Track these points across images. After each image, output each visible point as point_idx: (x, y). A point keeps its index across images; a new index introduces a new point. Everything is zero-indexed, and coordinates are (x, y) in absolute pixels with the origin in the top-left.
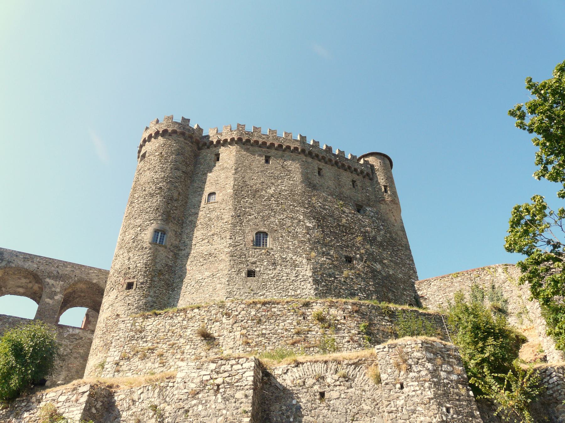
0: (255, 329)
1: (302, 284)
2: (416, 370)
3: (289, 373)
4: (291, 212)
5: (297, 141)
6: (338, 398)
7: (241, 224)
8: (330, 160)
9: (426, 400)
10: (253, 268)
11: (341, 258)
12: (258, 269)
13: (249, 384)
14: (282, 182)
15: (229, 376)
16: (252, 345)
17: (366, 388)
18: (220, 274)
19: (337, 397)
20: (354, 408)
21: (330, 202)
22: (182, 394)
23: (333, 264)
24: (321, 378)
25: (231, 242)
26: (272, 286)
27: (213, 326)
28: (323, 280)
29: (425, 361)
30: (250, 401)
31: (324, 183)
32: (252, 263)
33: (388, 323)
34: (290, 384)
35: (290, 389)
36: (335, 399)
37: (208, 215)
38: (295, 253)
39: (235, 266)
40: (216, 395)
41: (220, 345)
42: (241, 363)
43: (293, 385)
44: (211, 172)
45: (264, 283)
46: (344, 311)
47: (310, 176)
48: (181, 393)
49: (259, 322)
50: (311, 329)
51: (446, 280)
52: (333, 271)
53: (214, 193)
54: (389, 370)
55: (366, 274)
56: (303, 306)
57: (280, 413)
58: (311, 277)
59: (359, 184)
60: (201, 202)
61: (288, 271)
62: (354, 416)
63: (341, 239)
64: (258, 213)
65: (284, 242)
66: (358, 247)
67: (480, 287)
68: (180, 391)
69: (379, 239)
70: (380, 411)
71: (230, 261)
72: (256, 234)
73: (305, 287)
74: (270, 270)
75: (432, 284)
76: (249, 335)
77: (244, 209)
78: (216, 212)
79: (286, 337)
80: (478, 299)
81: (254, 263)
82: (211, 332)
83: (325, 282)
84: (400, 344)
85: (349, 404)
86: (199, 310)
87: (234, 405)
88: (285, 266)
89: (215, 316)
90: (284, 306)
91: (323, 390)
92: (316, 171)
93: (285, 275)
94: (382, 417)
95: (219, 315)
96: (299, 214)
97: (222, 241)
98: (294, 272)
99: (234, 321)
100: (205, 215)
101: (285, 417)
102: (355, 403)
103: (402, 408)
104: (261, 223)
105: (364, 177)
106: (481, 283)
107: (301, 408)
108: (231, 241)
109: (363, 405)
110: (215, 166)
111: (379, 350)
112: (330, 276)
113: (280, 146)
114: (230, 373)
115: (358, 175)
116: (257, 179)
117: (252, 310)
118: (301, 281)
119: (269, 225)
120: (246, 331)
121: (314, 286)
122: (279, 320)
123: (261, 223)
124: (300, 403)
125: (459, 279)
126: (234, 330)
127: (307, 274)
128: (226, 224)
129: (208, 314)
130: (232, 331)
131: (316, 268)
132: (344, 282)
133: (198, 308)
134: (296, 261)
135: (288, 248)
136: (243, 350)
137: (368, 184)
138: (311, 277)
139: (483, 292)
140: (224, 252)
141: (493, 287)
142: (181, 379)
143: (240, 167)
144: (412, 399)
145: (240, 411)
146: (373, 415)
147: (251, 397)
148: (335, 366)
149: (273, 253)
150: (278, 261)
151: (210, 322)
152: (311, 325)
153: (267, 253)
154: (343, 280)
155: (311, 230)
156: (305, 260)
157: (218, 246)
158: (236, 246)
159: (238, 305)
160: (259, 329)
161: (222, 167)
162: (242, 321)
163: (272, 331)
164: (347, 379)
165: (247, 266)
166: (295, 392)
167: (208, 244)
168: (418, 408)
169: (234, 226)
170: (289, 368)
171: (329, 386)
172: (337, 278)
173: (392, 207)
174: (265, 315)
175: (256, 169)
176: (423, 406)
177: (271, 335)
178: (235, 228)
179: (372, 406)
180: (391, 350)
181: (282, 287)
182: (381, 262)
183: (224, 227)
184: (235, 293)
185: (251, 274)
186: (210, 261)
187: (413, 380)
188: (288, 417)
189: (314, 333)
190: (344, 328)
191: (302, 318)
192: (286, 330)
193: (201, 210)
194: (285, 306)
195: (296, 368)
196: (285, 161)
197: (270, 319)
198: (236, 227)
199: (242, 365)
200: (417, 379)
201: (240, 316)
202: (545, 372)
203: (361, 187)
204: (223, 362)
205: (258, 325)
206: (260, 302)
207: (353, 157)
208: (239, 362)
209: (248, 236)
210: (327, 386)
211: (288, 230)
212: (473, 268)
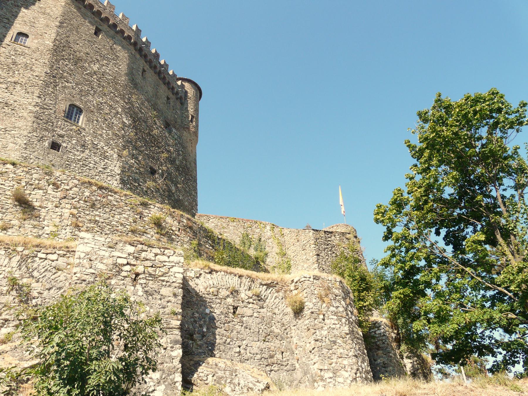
0: (88, 212)
1: (109, 178)
2: (335, 306)
3: (202, 278)
4: (111, 99)
5: (133, 30)
6: (251, 316)
7: (55, 86)
8: (155, 67)
9: (343, 335)
10: (60, 141)
11: (147, 167)
12: (64, 145)
13: (178, 281)
14: (107, 64)
15: (152, 267)
16: (82, 229)
17: (276, 311)
18: (16, 132)
19: (250, 315)
20: (266, 329)
21: (146, 107)
22: (87, 275)
23: (140, 170)
24: (235, 292)
25: (39, 101)
26: (77, 169)
27: (33, 193)
28: (128, 182)
29: (341, 299)
30: (180, 302)
31: (144, 86)
32: (58, 135)
33: (210, 247)
34: (203, 290)
35: (204, 296)
36: (249, 316)
37: (13, 57)
38: (108, 144)
39: (38, 130)
40: (134, 286)
41: (40, 218)
42: (168, 254)
43: (206, 293)
44: (27, 8)
45: (68, 163)
46: (179, 223)
47: (134, 72)
48: (85, 273)
49: (93, 206)
50: (146, 231)
51: (224, 221)
52: (139, 177)
53: (26, 36)
54: (314, 301)
55: (163, 191)
56: (141, 204)
57: (192, 320)
58: (119, 175)
59: (171, 101)
60: (5, 36)
61: (97, 159)
62: (266, 337)
63: (149, 148)
64: (77, 84)
65: (98, 127)
66: (161, 162)
67: (249, 236)
68: (84, 269)
69: (177, 162)
70: (288, 336)
71: (34, 122)
72: (70, 105)
73: (110, 182)
74: (78, 151)
75: (210, 220)
76: (80, 216)
77: (61, 72)
78: (25, 58)
79: (121, 232)
80: (246, 246)
81: (62, 136)
82: (30, 200)
83: (130, 185)
84: (323, 277)
85: (261, 324)
86: (15, 167)
87: (160, 302)
88: (95, 153)
89: (37, 182)
90: (121, 198)
91: (237, 305)
92: (141, 70)
93: (93, 162)
94: (290, 342)
95: (43, 183)
96: (118, 106)
97: (27, 95)
98: (103, 163)
99: (62, 196)
100: (8, 54)
101: (198, 325)
102: (267, 324)
103: (326, 338)
104: (78, 97)
105: (177, 99)
106: (251, 233)
107: (215, 319)
108: (39, 101)
109: (274, 327)
110: (34, 4)
111: (305, 279)
112: (135, 180)
113: (115, 26)
114: (154, 262)
115: (173, 94)
116: (82, 46)
117: (86, 190)
118: (107, 175)
119: (86, 102)
120: (77, 212)
121: (120, 185)
122: (114, 211)
123: (78, 97)
124: (213, 314)
125: (235, 224)
126: (61, 206)
127: (116, 171)
128: (37, 78)
129: (28, 176)
130: (59, 207)
131: (125, 168)
132: (146, 191)
133: (14, 164)
134: (107, 152)
135: (101, 135)
136: (71, 233)
137: (179, 107)
138: (119, 175)
139: (251, 241)
140: (27, 108)
141: (260, 240)
142: (84, 254)
143: (66, 23)
144: (333, 331)
145: (167, 310)
146: (282, 339)
147: (180, 298)
148: (249, 282)
149: (84, 134)
150: (88, 144)
151: (29, 187)
152: (147, 227)
153: (79, 132)
154: (145, 189)
155: (126, 126)
156: (116, 155)
157: (20, 99)
158: (44, 108)
159: (70, 178)
160: (92, 213)
161: (43, 10)
162: (73, 198)
163: (106, 221)
164: (260, 298)
165: (53, 136)
166: (208, 300)
167: (6, 91)
168: (338, 341)
169: (47, 85)
170: (201, 272)
171: (243, 302)
172: (140, 185)
173: (193, 138)
174: (100, 200)
175: (84, 35)
176: (341, 339)
177: (104, 224)
178: (47, 88)
179: (282, 330)
180: (315, 281)
181: (87, 173)
182: (176, 185)
183: (34, 80)
184: (32, 161)
185: (55, 146)
186: (4, 112)
187: (333, 314)
188: (201, 326)
189: (149, 236)
190: (178, 240)
191: (139, 216)
192: (122, 224)
193: (4, 46)
194: (123, 198)
195: (209, 275)
196: (115, 43)
197: (105, 207)
198: (49, 87)
199: (169, 257)
200: (336, 314)
201: (71, 192)
202: (375, 324)
203: (173, 106)
204: (145, 248)
205: (91, 209)
206: (96, 185)
207: (174, 75)
208: (165, 253)
209: (61, 103)
210: (240, 302)
211: (104, 117)
212: (248, 219)
